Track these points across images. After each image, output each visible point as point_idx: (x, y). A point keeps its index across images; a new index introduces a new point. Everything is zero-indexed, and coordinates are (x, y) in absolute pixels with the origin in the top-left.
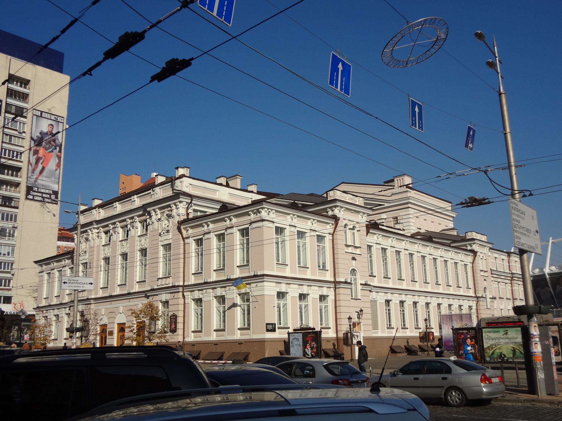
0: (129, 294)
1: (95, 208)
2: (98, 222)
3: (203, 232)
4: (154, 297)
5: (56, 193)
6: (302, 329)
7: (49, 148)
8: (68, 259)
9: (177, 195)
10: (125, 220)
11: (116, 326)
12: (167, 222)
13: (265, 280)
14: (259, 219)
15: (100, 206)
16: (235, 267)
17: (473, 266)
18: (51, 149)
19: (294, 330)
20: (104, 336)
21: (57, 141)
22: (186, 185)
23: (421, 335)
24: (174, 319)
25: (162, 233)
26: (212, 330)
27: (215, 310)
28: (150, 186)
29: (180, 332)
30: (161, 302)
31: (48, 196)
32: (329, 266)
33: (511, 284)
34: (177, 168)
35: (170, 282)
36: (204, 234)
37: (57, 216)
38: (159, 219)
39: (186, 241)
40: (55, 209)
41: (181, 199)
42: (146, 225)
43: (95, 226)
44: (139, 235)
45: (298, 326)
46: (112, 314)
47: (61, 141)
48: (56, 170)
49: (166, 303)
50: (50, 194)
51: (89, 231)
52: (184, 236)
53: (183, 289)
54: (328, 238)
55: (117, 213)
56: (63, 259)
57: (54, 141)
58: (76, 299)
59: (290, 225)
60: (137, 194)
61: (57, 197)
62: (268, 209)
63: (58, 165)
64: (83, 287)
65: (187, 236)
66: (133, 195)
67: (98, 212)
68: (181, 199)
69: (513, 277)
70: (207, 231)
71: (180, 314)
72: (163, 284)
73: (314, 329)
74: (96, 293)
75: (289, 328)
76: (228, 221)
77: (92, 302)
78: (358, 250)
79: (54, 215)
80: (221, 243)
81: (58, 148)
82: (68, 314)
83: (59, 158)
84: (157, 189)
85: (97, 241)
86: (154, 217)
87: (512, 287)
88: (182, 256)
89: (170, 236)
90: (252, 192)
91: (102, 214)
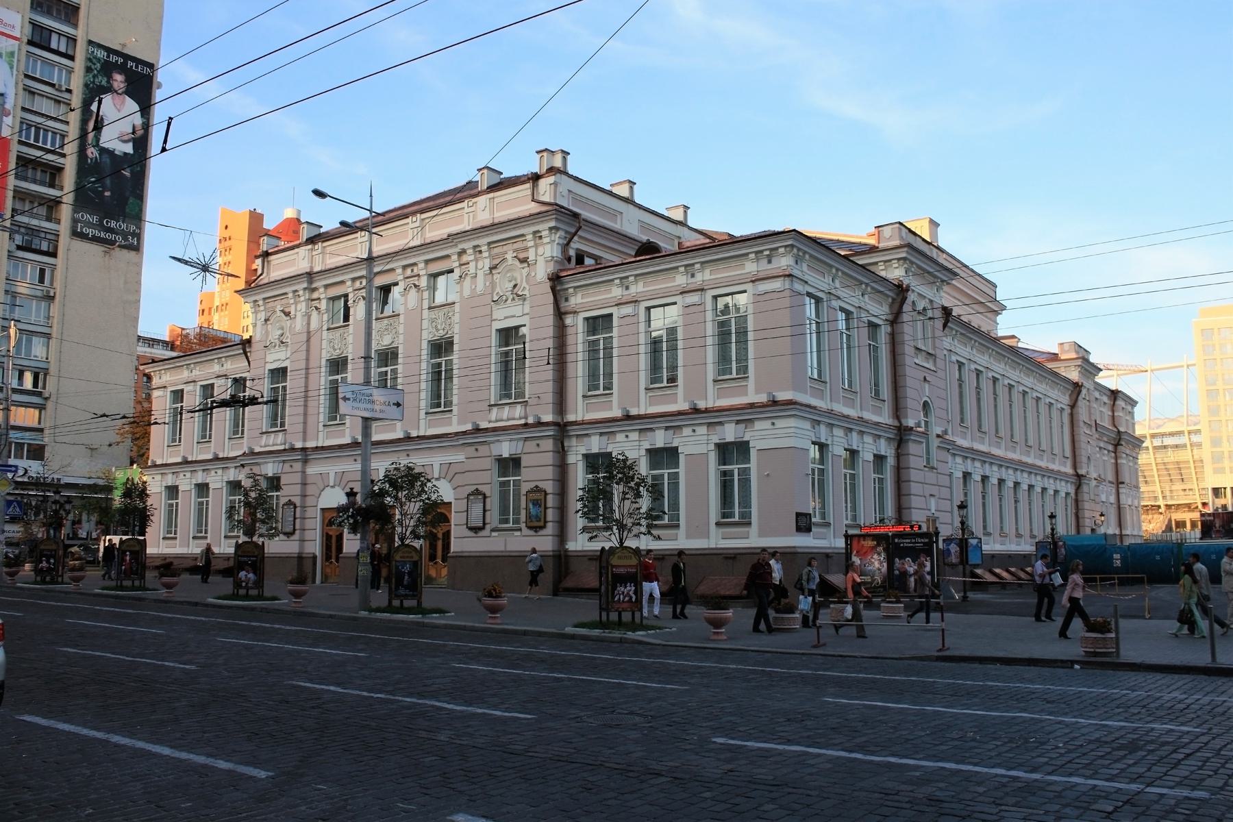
87: (1116, 458)
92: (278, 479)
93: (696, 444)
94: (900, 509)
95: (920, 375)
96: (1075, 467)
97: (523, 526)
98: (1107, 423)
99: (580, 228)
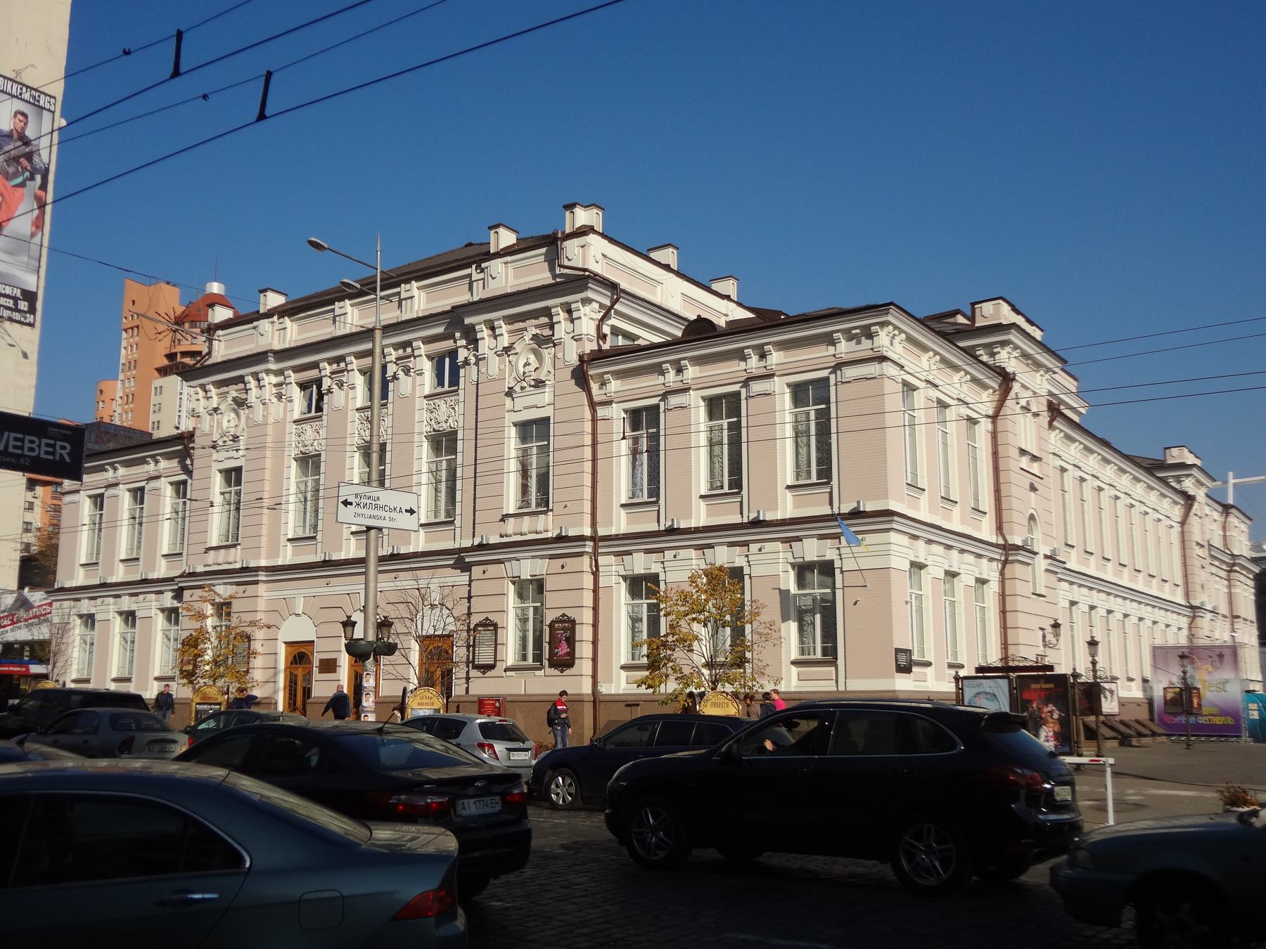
0: (327, 564)
1: (269, 315)
2: (282, 355)
3: (744, 376)
4: (490, 567)
5: (30, 296)
6: (1005, 670)
7: (16, 175)
8: (169, 456)
9: (580, 281)
10: (315, 365)
11: (282, 650)
12: (233, 415)
13: (894, 526)
14: (870, 354)
15: (282, 312)
16: (77, 565)
17: (1183, 532)
18: (20, 180)
19: (980, 669)
20: (300, 672)
21: (36, 159)
22: (594, 254)
23: (1170, 696)
24: (564, 629)
25: (517, 388)
26: (151, 678)
27: (159, 637)
28: (480, 256)
29: (584, 666)
30: (514, 583)
31: (10, 303)
32: (987, 503)
33: (1229, 580)
34: (570, 207)
35: (236, 559)
36: (664, 396)
37: (34, 357)
38: (216, 410)
39: (601, 412)
40: (29, 338)
41: (590, 294)
42: (448, 371)
43: (273, 366)
44: (427, 392)
45: (994, 658)
46: (282, 611)
47: (46, 160)
48: (33, 235)
49: (223, 608)
50: (15, 299)
51: (249, 379)
52: (596, 399)
53: (595, 548)
54: (985, 426)
55: (347, 331)
56: (153, 457)
57: (29, 156)
58: (372, 555)
59: (928, 382)
60: (418, 279)
61: (32, 310)
62: (896, 328)
63: (38, 224)
64: (391, 519)
65: (603, 398)
66: (408, 281)
67: (277, 326)
68: (590, 294)
69: (1234, 565)
70: (112, 481)
71: (587, 616)
72: (220, 561)
73: (1051, 668)
74: (274, 552)
75: (962, 666)
76: (672, 372)
77: (262, 576)
78: (1036, 465)
79: (25, 356)
80: (310, 479)
81: (38, 178)
82: (172, 614)
83: (42, 206)
84: (496, 266)
85: (276, 409)
86: (486, 343)
87: (1229, 587)
88: (588, 452)
89: (547, 396)
90: (728, 298)
91: (292, 333)
92: (229, 604)
93: (771, 567)
94: (1005, 645)
95: (1026, 481)
96: (1187, 595)
97: (546, 663)
98: (1217, 542)
99: (617, 300)
